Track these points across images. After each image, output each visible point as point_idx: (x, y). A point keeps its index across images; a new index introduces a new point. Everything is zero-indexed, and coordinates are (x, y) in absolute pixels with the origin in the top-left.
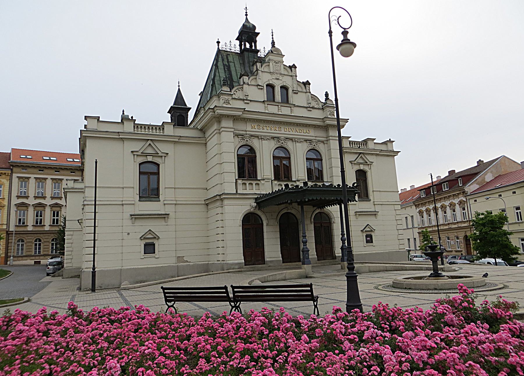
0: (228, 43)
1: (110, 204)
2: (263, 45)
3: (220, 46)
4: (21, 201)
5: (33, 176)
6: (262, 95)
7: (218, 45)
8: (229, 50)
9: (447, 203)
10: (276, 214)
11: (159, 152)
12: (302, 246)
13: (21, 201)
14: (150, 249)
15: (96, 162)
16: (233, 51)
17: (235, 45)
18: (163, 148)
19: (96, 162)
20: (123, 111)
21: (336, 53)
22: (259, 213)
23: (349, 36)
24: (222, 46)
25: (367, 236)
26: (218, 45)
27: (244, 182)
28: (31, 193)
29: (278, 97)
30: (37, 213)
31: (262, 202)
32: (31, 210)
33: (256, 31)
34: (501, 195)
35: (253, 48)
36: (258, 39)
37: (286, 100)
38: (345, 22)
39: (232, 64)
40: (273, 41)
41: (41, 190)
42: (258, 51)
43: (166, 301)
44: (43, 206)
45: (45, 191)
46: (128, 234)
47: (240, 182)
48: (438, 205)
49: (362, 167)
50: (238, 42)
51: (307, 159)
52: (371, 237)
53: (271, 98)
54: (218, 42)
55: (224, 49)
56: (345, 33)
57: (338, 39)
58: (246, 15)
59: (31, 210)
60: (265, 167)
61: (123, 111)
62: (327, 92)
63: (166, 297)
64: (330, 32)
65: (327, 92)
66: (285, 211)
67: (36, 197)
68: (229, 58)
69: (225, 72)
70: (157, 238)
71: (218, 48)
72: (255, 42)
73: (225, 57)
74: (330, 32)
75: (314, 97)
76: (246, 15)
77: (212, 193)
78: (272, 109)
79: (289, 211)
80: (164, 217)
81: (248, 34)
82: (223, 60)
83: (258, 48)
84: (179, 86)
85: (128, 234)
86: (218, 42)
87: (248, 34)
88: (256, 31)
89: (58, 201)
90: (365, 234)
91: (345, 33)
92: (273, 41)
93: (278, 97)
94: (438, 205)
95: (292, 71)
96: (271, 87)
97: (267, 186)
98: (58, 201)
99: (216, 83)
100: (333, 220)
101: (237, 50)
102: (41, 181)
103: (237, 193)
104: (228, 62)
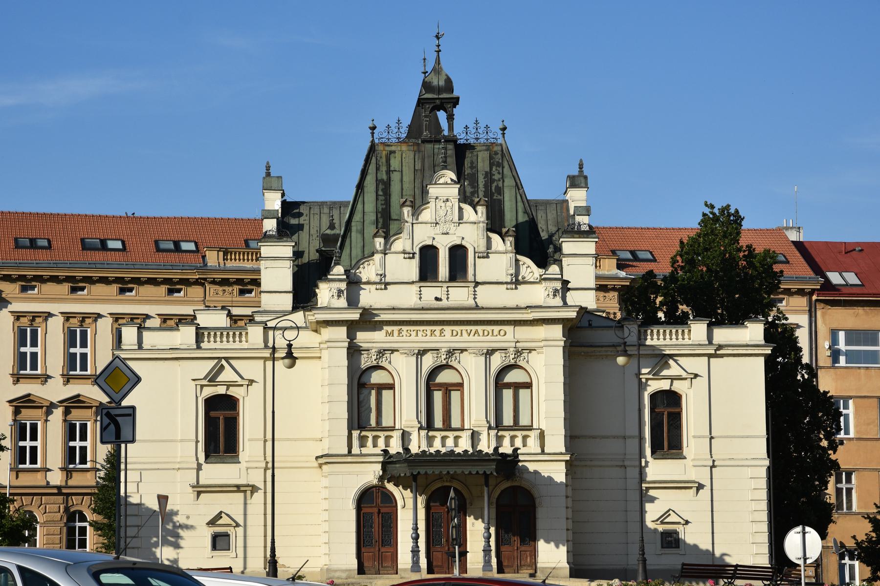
3: (376, 136)
6: (412, 269)
7: (373, 134)
20: (268, 168)
26: (373, 134)
39: (395, 177)
47: (356, 433)
60: (403, 408)
61: (268, 168)
68: (392, 162)
69: (377, 199)
71: (373, 141)
73: (384, 160)
78: (430, 293)
81: (437, 98)
82: (377, 169)
86: (373, 128)
88: (456, 93)
93: (443, 269)
95: (476, 212)
99: (354, 229)
100: (537, 501)
102: (513, 438)
104: (389, 172)
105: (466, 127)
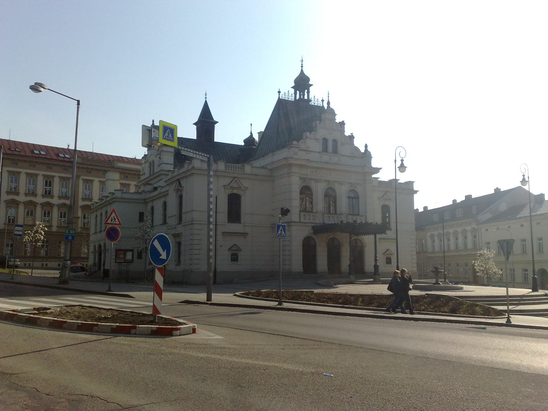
0: (287, 93)
4: (11, 197)
5: (24, 171)
8: (287, 99)
11: (242, 187)
13: (11, 197)
14: (235, 258)
20: (153, 121)
21: (397, 169)
22: (314, 237)
23: (404, 162)
24: (282, 96)
25: (232, 255)
28: (22, 189)
29: (330, 149)
30: (45, 212)
32: (21, 208)
33: (310, 83)
34: (509, 227)
36: (310, 88)
37: (335, 151)
38: (403, 155)
40: (328, 101)
41: (31, 187)
44: (34, 204)
45: (8, 184)
51: (348, 197)
52: (236, 255)
53: (325, 150)
54: (279, 92)
56: (402, 161)
57: (399, 164)
58: (302, 67)
59: (21, 208)
61: (153, 121)
62: (366, 145)
64: (395, 161)
65: (366, 145)
66: (332, 236)
67: (26, 195)
70: (240, 250)
74: (395, 161)
76: (302, 67)
77: (223, 207)
80: (245, 234)
81: (302, 83)
86: (279, 92)
87: (302, 83)
89: (50, 200)
90: (385, 257)
91: (402, 161)
92: (328, 101)
96: (325, 140)
98: (50, 200)
103: (300, 222)
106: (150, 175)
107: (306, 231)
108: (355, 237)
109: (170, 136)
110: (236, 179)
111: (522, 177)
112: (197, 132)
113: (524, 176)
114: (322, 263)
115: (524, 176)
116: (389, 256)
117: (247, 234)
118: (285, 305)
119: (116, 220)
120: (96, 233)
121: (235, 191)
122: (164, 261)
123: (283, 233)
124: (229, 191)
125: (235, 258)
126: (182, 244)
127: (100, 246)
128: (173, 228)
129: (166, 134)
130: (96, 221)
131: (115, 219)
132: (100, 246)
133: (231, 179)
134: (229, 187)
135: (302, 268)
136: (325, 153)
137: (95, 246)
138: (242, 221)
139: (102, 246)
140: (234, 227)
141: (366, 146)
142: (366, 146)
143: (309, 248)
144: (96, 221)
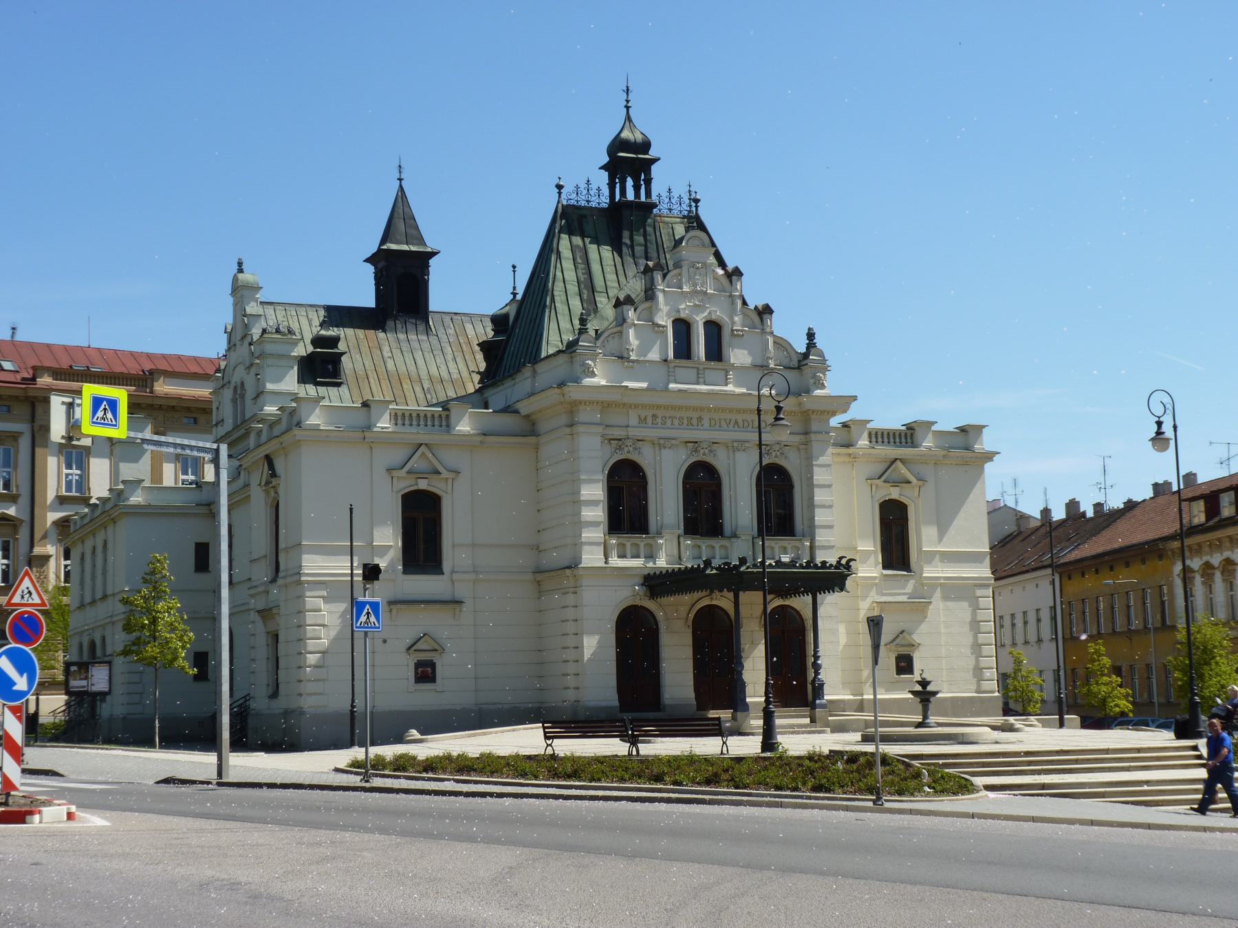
0: (583, 186)
1: (230, 546)
2: (667, 183)
3: (563, 196)
6: (662, 348)
7: (560, 193)
8: (583, 203)
9: (1216, 560)
10: (688, 608)
11: (441, 469)
12: (811, 674)
14: (425, 673)
15: (351, 510)
16: (594, 204)
17: (599, 189)
18: (451, 458)
19: (351, 510)
22: (650, 604)
24: (569, 197)
25: (419, 665)
26: (560, 193)
27: (621, 540)
31: (657, 584)
35: (643, 199)
42: (655, 206)
43: (546, 738)
46: (385, 641)
48: (1195, 563)
49: (894, 493)
50: (605, 175)
52: (432, 665)
54: (559, 187)
55: (572, 202)
60: (666, 500)
63: (545, 733)
72: (648, 182)
75: (781, 344)
76: (628, 108)
79: (714, 602)
81: (629, 160)
83: (654, 198)
84: (400, 180)
85: (385, 641)
87: (629, 160)
94: (1195, 563)
97: (668, 552)
101: (604, 201)
105: (577, 187)
106: (236, 427)
107: (629, 594)
108: (778, 602)
109: (109, 415)
110: (422, 449)
111: (1155, 428)
112: (377, 285)
113: (1159, 424)
114: (678, 676)
115: (1159, 424)
116: (904, 651)
117: (460, 602)
118: (377, 782)
119: (35, 595)
120: (82, 606)
121: (423, 485)
122: (22, 694)
123: (373, 619)
124: (406, 484)
125: (425, 673)
126: (281, 638)
127: (93, 645)
128: (258, 594)
129: (100, 414)
130: (83, 571)
131: (30, 593)
132: (93, 645)
133: (409, 451)
134: (403, 473)
135: (693, 695)
136: (684, 362)
137: (81, 645)
138: (446, 566)
139: (98, 643)
140: (423, 585)
141: (811, 335)
142: (811, 335)
143: (635, 635)
144: (83, 571)
